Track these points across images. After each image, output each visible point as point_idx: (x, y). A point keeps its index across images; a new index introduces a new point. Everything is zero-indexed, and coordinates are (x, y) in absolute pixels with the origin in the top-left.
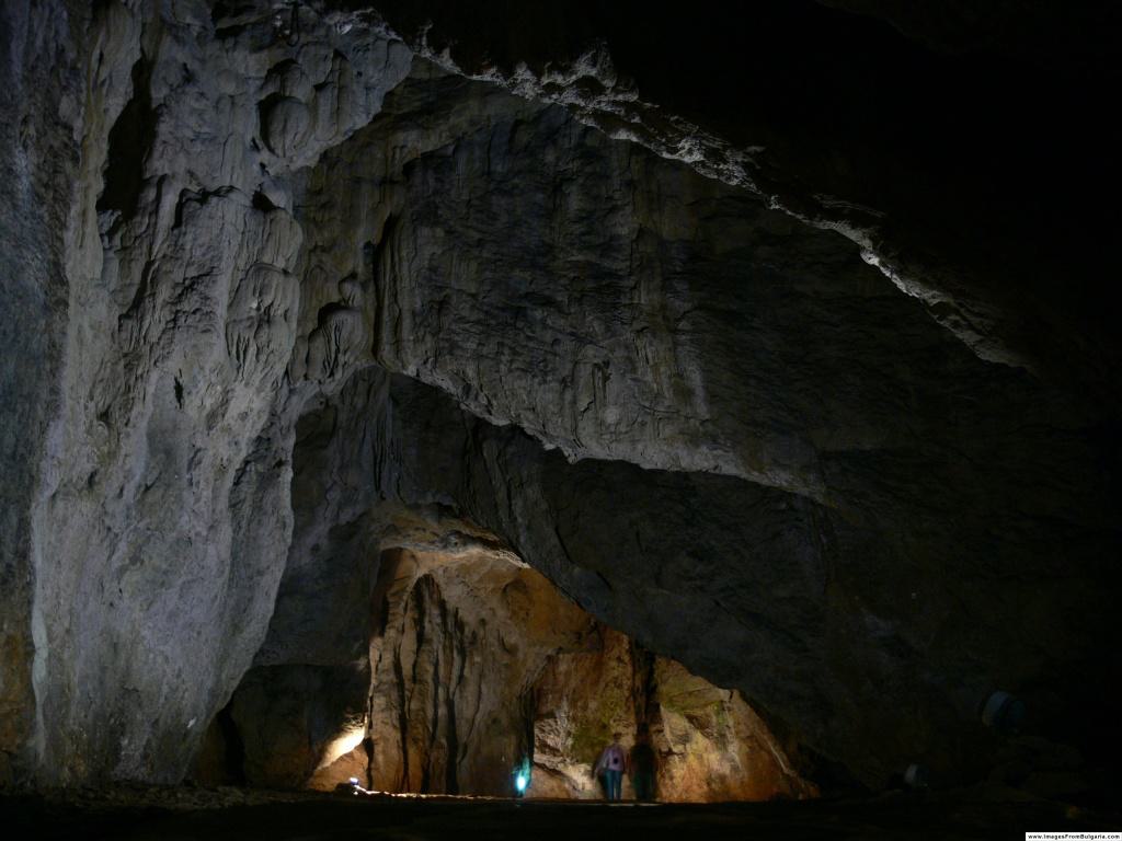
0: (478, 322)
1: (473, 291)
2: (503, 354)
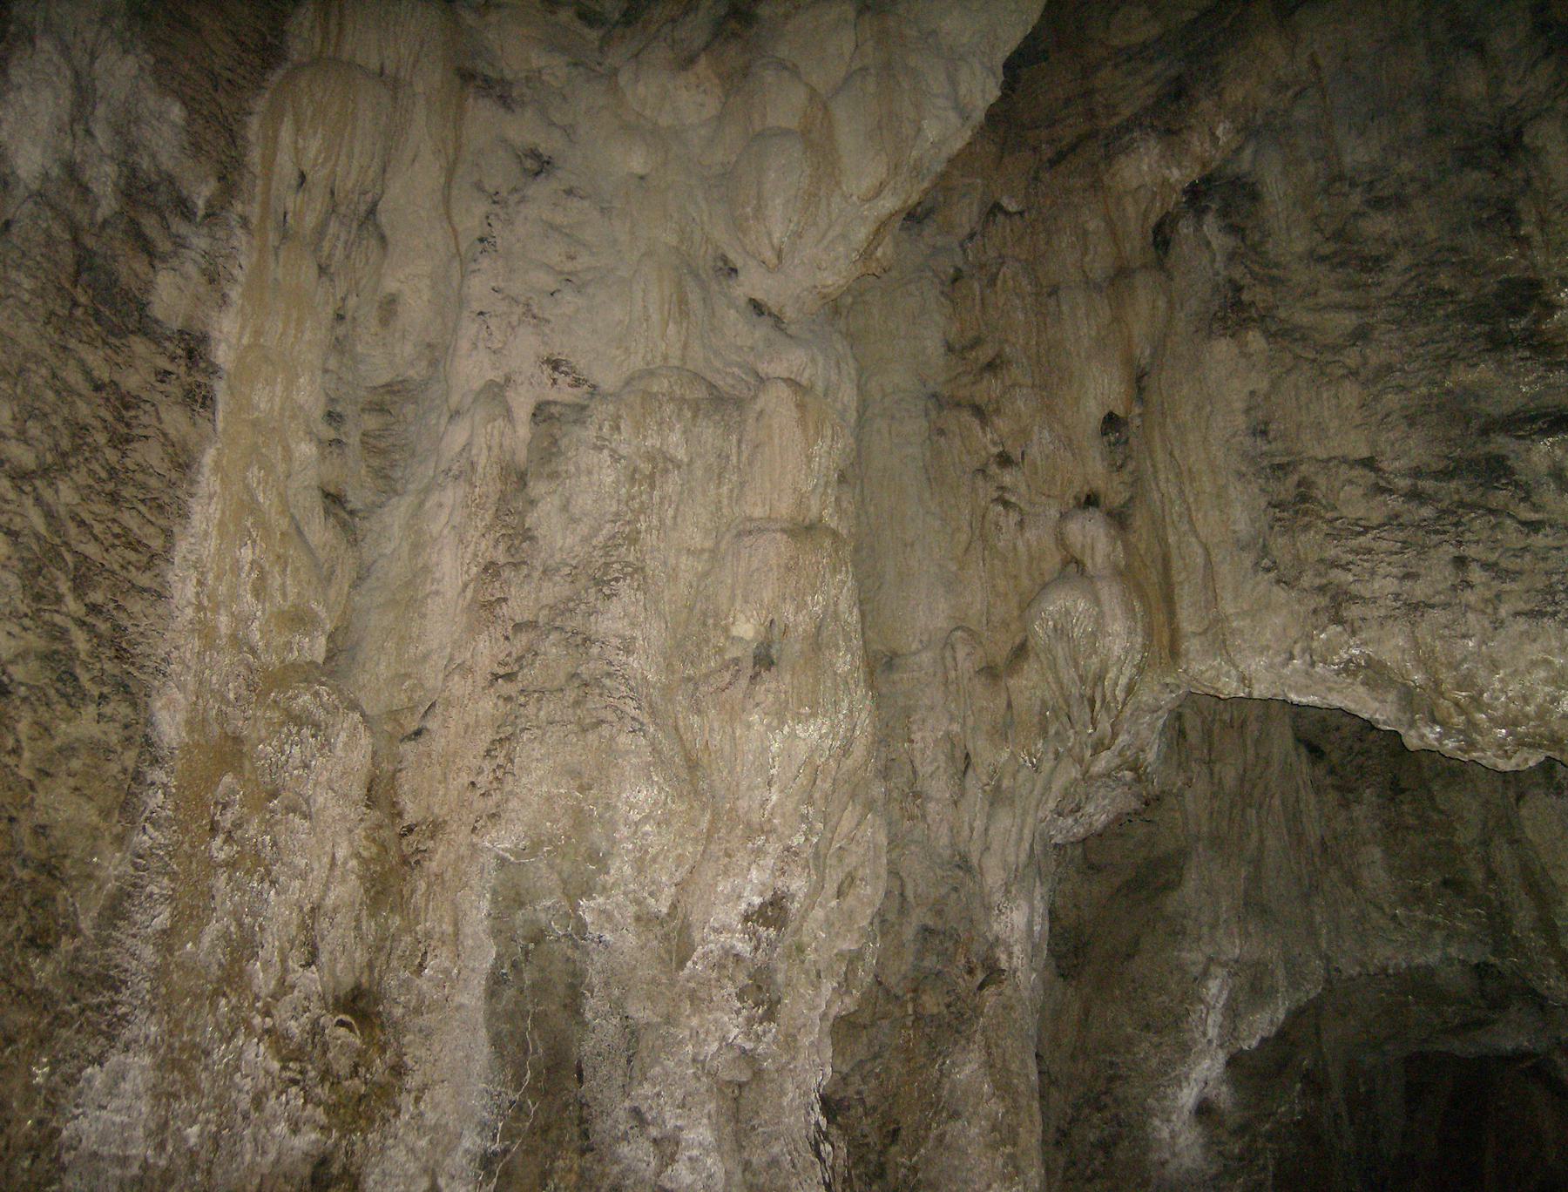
0: (1393, 520)
1: (1364, 452)
2: (1469, 585)
